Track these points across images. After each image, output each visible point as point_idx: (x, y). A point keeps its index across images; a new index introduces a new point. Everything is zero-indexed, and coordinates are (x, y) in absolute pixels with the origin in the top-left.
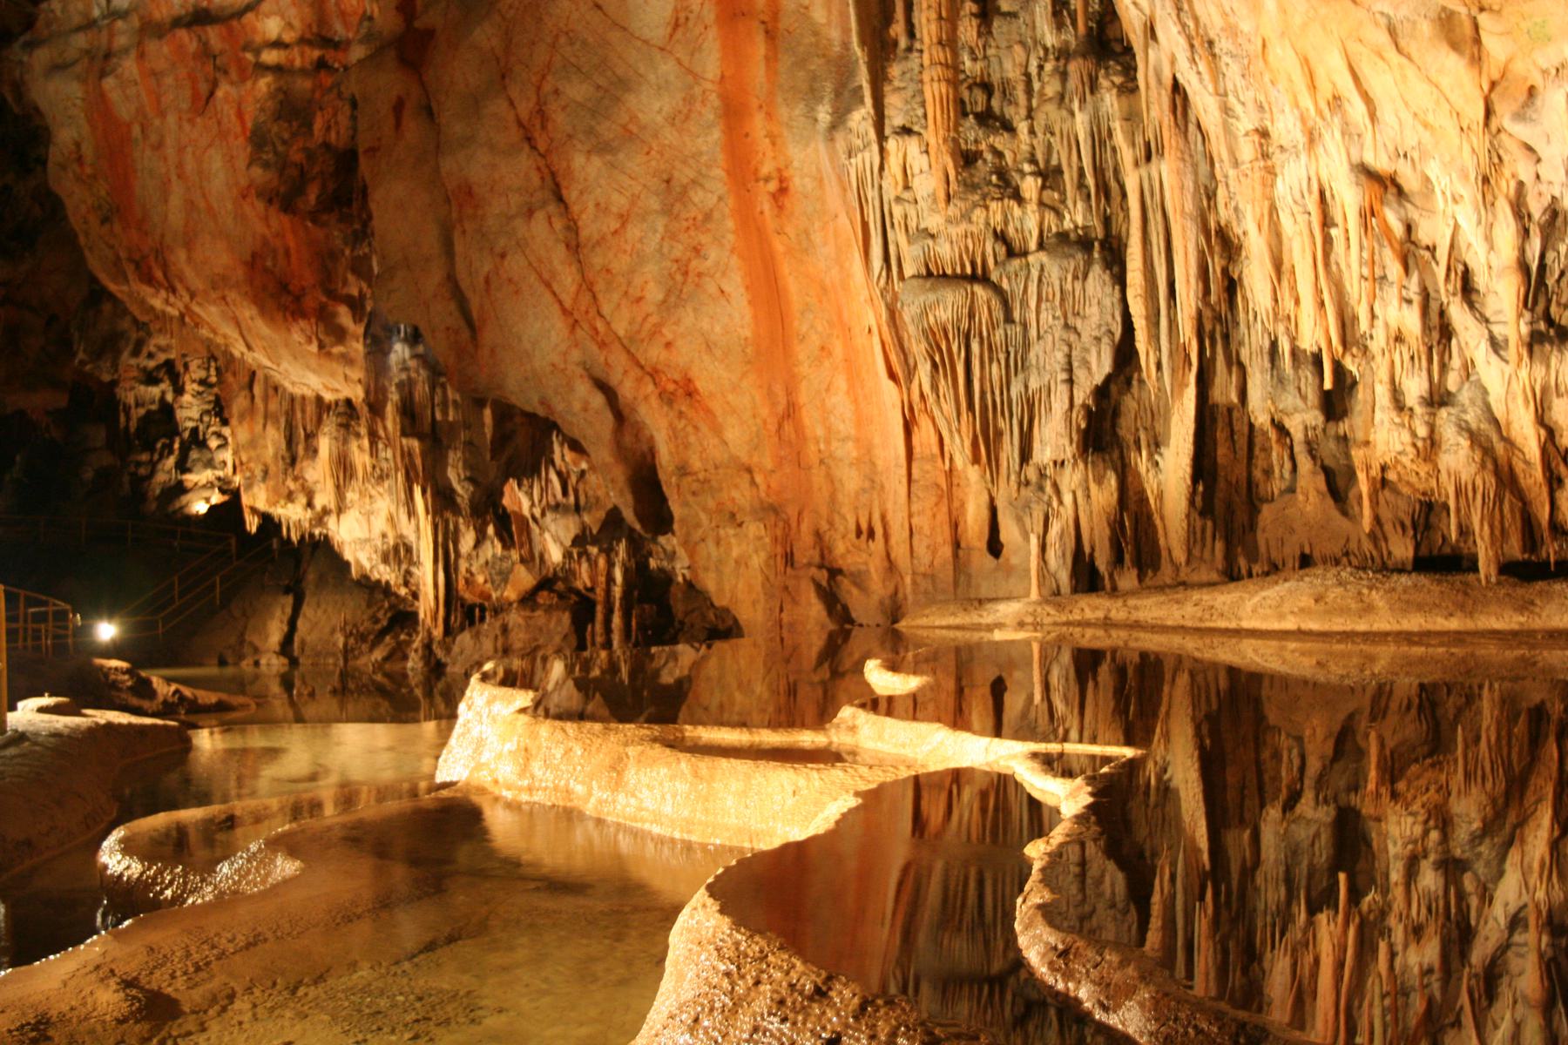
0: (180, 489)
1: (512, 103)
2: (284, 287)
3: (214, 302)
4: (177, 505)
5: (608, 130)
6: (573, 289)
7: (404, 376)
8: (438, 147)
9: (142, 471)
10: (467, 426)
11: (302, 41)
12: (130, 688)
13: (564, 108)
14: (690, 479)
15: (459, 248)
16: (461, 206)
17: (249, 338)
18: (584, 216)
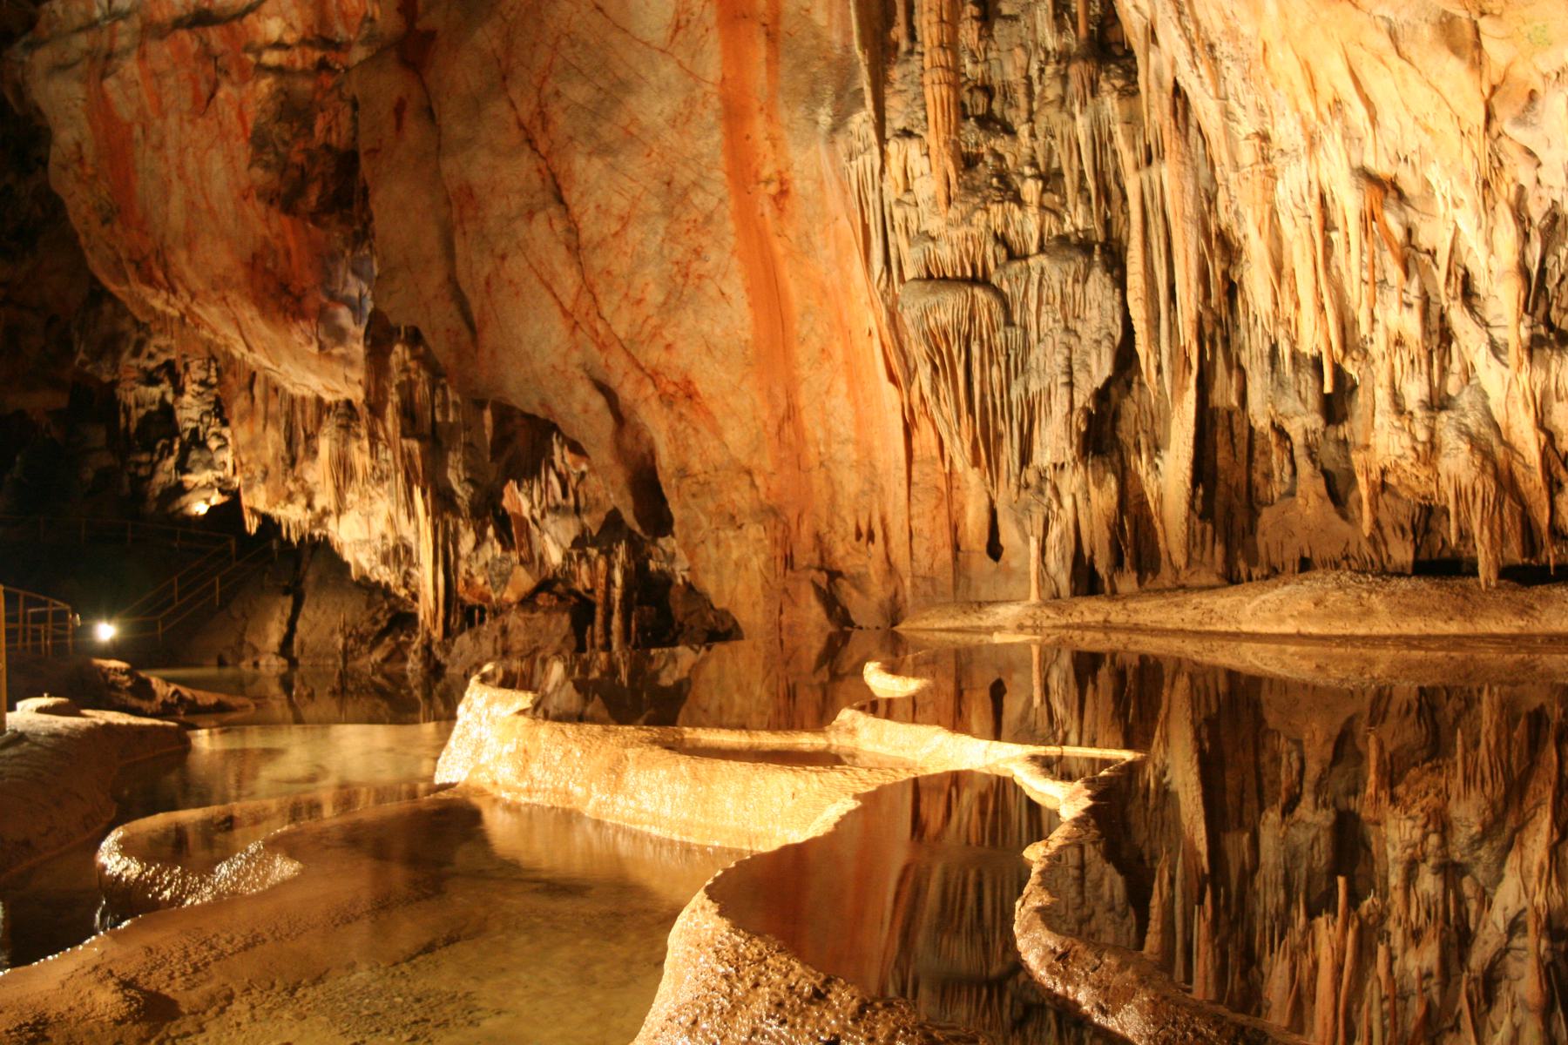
0: (180, 490)
1: (513, 105)
2: (284, 288)
5: (607, 132)
6: (574, 290)
7: (404, 378)
8: (439, 147)
9: (142, 472)
10: (468, 428)
11: (304, 42)
14: (689, 481)
16: (461, 207)
17: (249, 338)
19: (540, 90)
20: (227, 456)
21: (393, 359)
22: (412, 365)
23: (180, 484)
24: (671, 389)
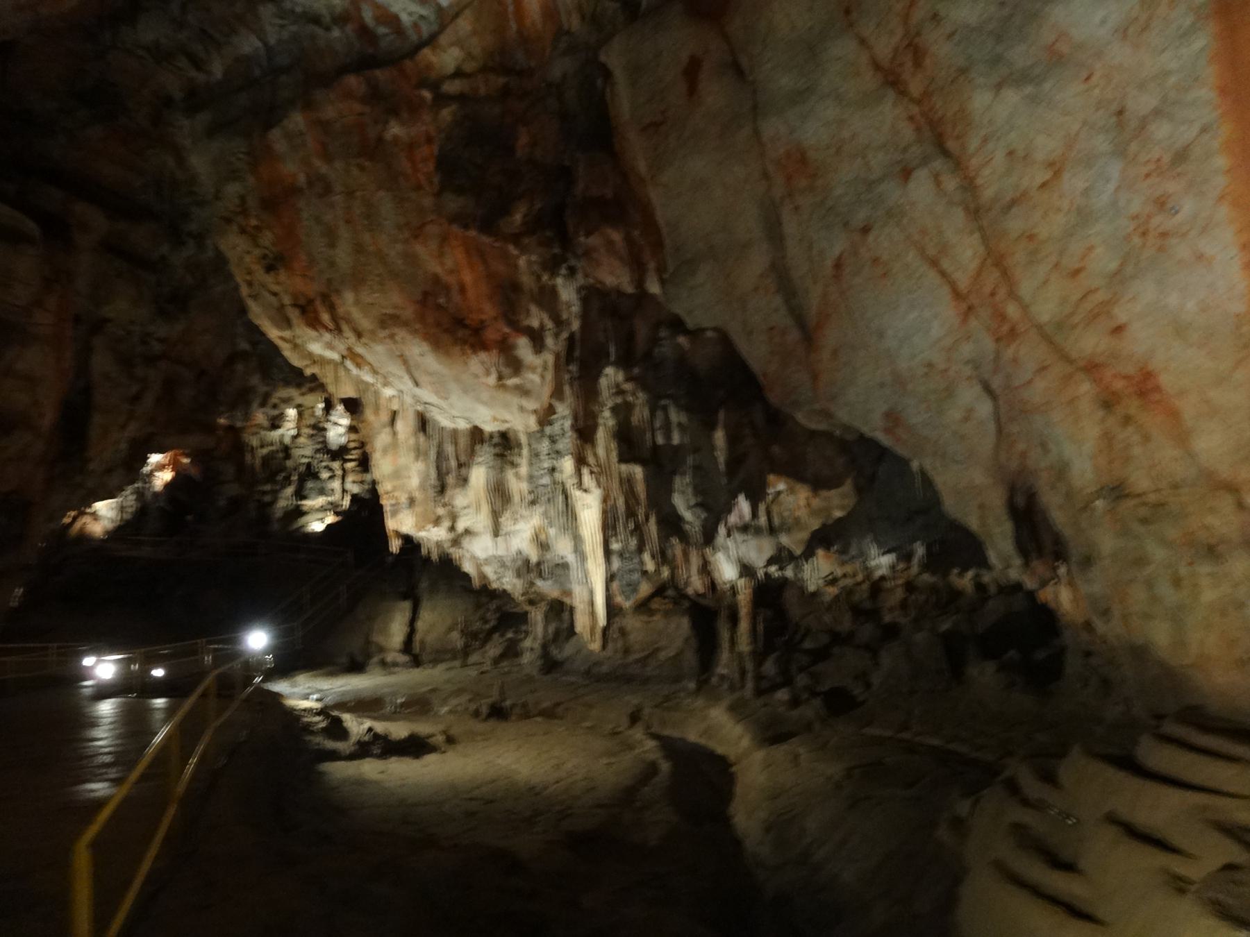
0: (299, 513)
1: (863, 42)
2: (459, 322)
3: (381, 341)
4: (295, 526)
5: (1020, 55)
6: (974, 265)
7: (619, 400)
8: (755, 108)
9: (267, 498)
10: (696, 450)
11: (484, 69)
12: (323, 729)
13: (950, 36)
14: (1131, 503)
15: (790, 226)
16: (789, 178)
17: (417, 374)
18: (986, 172)
19: (906, 18)
20: (336, 484)
21: (603, 382)
22: (628, 386)
23: (298, 507)
24: (1119, 385)
